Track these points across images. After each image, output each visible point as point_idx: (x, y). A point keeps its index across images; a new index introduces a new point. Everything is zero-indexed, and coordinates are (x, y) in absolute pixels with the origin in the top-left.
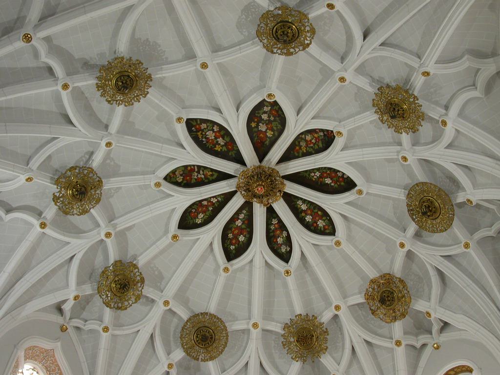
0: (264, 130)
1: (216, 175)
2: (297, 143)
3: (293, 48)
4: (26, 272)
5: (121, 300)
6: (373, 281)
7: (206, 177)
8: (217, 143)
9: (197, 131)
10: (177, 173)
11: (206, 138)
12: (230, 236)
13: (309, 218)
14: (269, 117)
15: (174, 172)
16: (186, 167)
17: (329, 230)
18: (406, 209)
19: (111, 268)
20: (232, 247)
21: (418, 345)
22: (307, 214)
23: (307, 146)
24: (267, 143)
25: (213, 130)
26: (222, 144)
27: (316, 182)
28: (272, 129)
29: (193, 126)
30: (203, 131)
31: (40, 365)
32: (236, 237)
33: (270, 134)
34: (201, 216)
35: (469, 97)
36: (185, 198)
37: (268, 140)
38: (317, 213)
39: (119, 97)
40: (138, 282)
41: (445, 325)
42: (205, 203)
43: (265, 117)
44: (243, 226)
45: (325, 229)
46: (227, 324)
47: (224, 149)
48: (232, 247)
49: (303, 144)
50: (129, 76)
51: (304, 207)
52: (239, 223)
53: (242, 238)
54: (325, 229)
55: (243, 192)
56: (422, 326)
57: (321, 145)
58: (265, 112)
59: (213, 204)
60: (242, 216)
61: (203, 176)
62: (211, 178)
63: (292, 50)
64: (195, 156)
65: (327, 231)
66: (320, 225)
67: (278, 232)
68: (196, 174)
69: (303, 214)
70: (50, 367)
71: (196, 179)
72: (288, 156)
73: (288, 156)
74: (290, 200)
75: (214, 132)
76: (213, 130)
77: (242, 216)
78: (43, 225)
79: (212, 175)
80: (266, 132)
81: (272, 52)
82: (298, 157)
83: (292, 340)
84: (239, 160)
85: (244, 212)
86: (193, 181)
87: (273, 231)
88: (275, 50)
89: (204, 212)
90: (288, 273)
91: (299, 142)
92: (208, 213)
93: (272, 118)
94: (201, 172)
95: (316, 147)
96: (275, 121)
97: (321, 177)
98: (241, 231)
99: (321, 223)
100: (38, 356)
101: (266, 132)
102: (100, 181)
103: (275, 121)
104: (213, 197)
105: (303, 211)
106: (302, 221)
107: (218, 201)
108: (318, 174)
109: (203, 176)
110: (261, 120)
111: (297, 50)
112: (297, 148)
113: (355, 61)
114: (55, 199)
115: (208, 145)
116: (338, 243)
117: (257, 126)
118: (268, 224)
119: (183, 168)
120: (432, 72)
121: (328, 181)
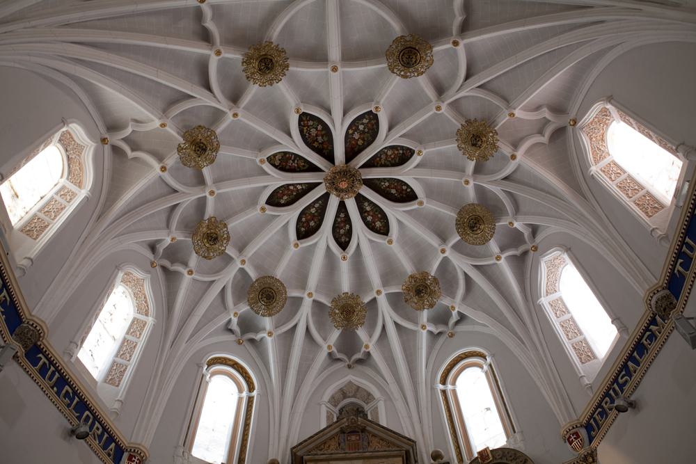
0: (357, 138)
1: (307, 166)
2: (379, 155)
3: (410, 72)
4: (353, 106)
5: (208, 250)
6: (411, 277)
7: (298, 167)
8: (317, 140)
9: (304, 126)
10: (277, 157)
11: (310, 134)
12: (304, 219)
13: (369, 218)
14: (364, 128)
15: (275, 155)
16: (285, 153)
17: (384, 230)
18: (454, 222)
19: (207, 222)
20: (303, 229)
21: (436, 331)
22: (369, 215)
23: (386, 159)
24: (356, 149)
25: (316, 129)
26: (320, 142)
27: (384, 190)
28: (363, 140)
29: (304, 121)
30: (308, 126)
31: (130, 290)
32: (308, 221)
33: (360, 142)
34: (285, 197)
35: (538, 141)
36: (279, 179)
37: (358, 146)
38: (377, 215)
39: (257, 76)
40: (224, 239)
41: (462, 318)
42: (291, 188)
43: (361, 127)
44: (316, 214)
45: (380, 229)
46: (287, 290)
47: (321, 146)
48: (303, 229)
49: (383, 157)
50: (271, 60)
51: (368, 209)
52: (313, 210)
53: (312, 224)
54: (380, 229)
55: (328, 184)
56: (442, 318)
57: (397, 161)
58: (363, 124)
59: (298, 190)
60: (317, 205)
61: (296, 165)
62: (302, 168)
63: (408, 74)
64: (298, 147)
65: (382, 231)
66: (378, 226)
67: (342, 225)
68: (291, 162)
69: (366, 214)
70: (137, 294)
71: (290, 166)
72: (370, 164)
73: (370, 164)
74: (360, 200)
75: (317, 130)
76: (316, 129)
77: (317, 205)
78: (163, 169)
79: (304, 166)
80: (358, 140)
81: (393, 72)
82: (376, 167)
83: (337, 311)
84: (330, 157)
85: (320, 202)
86: (288, 167)
87: (339, 223)
88: (395, 70)
89: (288, 195)
90: (344, 258)
91: (381, 155)
92: (291, 197)
93: (366, 130)
94: (296, 161)
95: (393, 162)
96: (368, 133)
97: (388, 187)
98: (313, 216)
99: (378, 224)
100: (130, 282)
101: (358, 140)
102: (218, 145)
103: (368, 133)
104: (299, 184)
105: (366, 211)
106: (364, 219)
107: (302, 189)
108: (387, 184)
109: (296, 165)
110: (357, 129)
111: (413, 75)
112: (378, 159)
113: (452, 96)
114: (180, 149)
115: (309, 139)
116: (390, 242)
117: (353, 133)
118: (337, 216)
119: (283, 154)
120: (516, 115)
121: (393, 191)
